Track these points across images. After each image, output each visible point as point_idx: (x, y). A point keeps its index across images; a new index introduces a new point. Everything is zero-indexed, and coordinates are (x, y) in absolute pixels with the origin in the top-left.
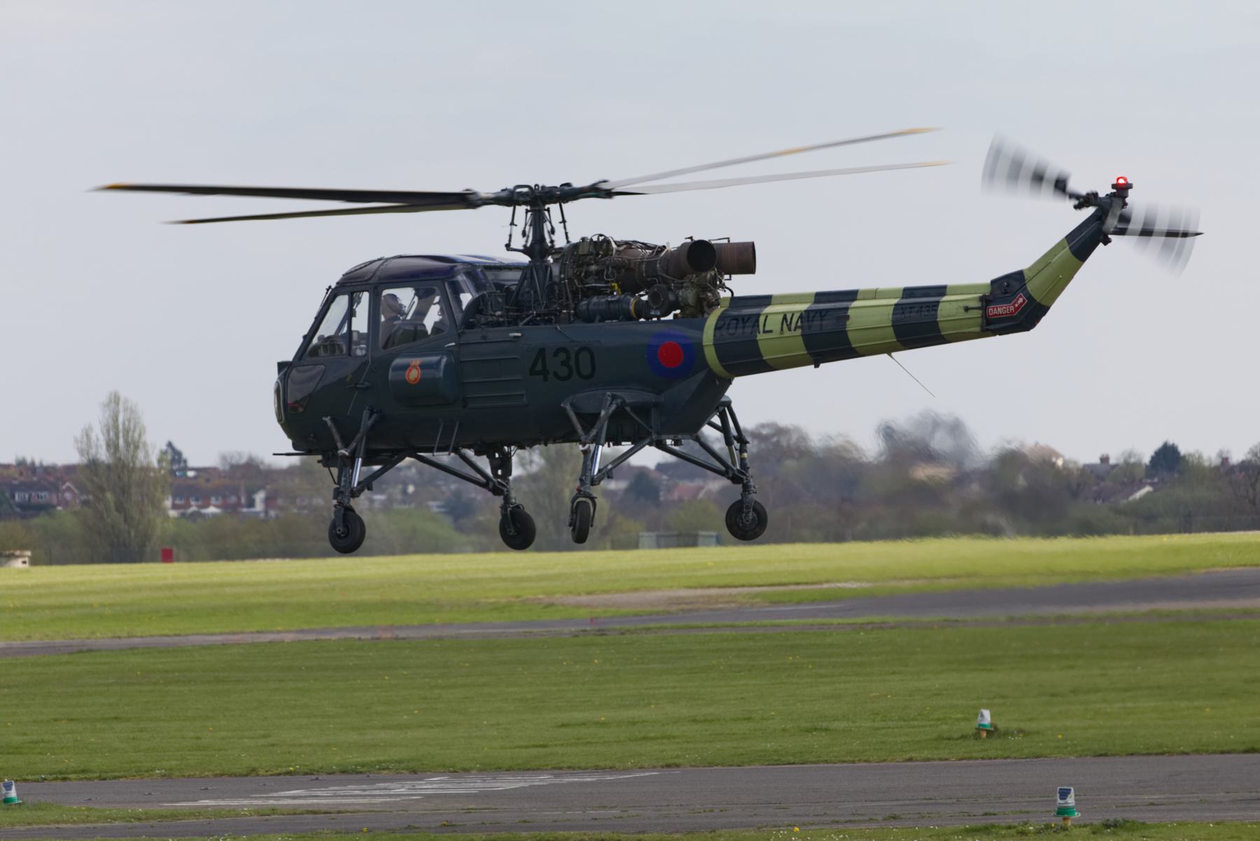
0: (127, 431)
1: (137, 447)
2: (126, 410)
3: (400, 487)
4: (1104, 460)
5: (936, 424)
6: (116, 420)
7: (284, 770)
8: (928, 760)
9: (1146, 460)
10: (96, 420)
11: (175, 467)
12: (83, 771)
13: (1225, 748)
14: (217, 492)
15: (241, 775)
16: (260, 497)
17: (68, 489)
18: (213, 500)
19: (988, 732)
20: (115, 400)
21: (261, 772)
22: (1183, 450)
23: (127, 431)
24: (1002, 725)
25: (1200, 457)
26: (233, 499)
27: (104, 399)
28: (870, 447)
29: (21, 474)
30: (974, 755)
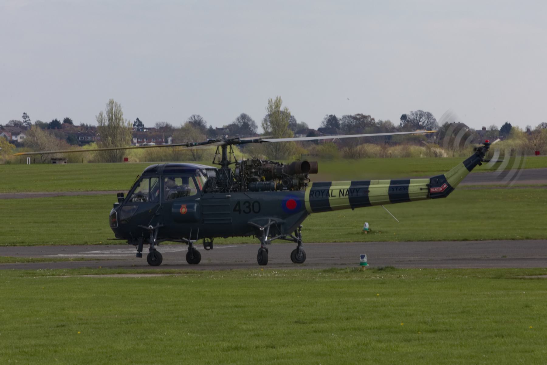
0: (116, 116)
1: (120, 120)
2: (116, 106)
3: (222, 136)
4: (484, 129)
5: (422, 114)
6: (112, 110)
7: (98, 243)
8: (342, 242)
9: (499, 129)
10: (105, 110)
11: (140, 127)
12: (22, 243)
13: (455, 239)
14: (155, 138)
15: (81, 245)
16: (170, 139)
17: (99, 135)
18: (152, 140)
19: (368, 232)
20: (112, 102)
21: (89, 243)
22: (513, 125)
23: (116, 116)
24: (375, 228)
25: (518, 128)
26: (160, 140)
27: (108, 102)
28: (397, 122)
29: (82, 130)
30: (360, 240)
